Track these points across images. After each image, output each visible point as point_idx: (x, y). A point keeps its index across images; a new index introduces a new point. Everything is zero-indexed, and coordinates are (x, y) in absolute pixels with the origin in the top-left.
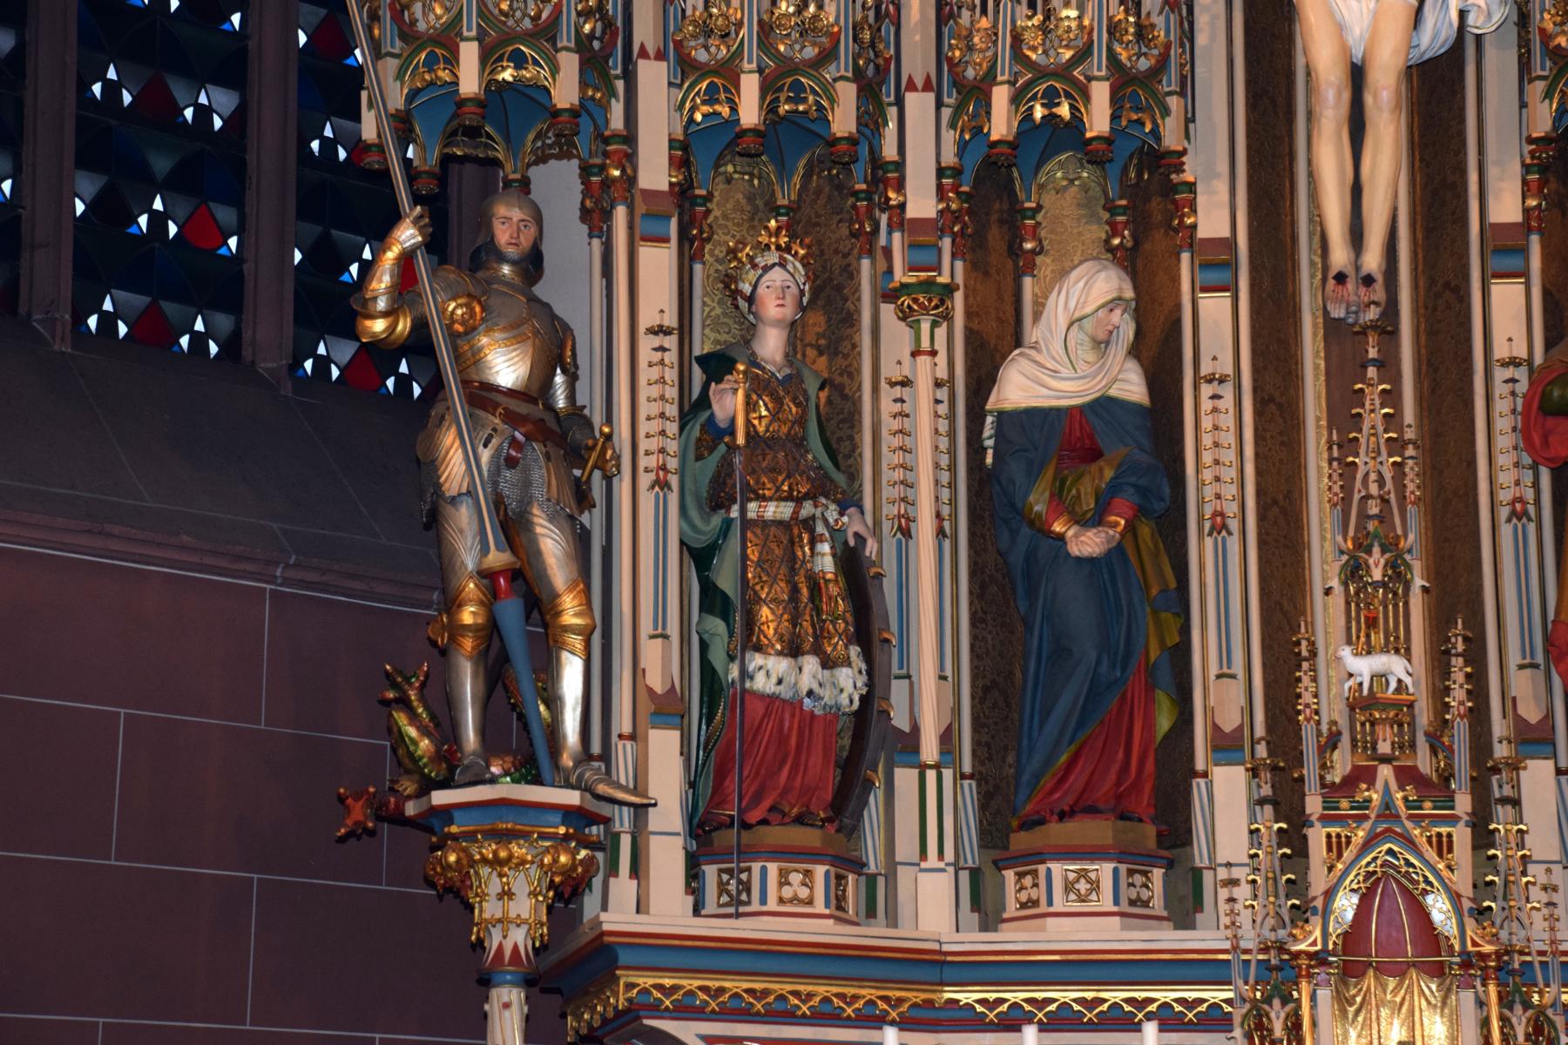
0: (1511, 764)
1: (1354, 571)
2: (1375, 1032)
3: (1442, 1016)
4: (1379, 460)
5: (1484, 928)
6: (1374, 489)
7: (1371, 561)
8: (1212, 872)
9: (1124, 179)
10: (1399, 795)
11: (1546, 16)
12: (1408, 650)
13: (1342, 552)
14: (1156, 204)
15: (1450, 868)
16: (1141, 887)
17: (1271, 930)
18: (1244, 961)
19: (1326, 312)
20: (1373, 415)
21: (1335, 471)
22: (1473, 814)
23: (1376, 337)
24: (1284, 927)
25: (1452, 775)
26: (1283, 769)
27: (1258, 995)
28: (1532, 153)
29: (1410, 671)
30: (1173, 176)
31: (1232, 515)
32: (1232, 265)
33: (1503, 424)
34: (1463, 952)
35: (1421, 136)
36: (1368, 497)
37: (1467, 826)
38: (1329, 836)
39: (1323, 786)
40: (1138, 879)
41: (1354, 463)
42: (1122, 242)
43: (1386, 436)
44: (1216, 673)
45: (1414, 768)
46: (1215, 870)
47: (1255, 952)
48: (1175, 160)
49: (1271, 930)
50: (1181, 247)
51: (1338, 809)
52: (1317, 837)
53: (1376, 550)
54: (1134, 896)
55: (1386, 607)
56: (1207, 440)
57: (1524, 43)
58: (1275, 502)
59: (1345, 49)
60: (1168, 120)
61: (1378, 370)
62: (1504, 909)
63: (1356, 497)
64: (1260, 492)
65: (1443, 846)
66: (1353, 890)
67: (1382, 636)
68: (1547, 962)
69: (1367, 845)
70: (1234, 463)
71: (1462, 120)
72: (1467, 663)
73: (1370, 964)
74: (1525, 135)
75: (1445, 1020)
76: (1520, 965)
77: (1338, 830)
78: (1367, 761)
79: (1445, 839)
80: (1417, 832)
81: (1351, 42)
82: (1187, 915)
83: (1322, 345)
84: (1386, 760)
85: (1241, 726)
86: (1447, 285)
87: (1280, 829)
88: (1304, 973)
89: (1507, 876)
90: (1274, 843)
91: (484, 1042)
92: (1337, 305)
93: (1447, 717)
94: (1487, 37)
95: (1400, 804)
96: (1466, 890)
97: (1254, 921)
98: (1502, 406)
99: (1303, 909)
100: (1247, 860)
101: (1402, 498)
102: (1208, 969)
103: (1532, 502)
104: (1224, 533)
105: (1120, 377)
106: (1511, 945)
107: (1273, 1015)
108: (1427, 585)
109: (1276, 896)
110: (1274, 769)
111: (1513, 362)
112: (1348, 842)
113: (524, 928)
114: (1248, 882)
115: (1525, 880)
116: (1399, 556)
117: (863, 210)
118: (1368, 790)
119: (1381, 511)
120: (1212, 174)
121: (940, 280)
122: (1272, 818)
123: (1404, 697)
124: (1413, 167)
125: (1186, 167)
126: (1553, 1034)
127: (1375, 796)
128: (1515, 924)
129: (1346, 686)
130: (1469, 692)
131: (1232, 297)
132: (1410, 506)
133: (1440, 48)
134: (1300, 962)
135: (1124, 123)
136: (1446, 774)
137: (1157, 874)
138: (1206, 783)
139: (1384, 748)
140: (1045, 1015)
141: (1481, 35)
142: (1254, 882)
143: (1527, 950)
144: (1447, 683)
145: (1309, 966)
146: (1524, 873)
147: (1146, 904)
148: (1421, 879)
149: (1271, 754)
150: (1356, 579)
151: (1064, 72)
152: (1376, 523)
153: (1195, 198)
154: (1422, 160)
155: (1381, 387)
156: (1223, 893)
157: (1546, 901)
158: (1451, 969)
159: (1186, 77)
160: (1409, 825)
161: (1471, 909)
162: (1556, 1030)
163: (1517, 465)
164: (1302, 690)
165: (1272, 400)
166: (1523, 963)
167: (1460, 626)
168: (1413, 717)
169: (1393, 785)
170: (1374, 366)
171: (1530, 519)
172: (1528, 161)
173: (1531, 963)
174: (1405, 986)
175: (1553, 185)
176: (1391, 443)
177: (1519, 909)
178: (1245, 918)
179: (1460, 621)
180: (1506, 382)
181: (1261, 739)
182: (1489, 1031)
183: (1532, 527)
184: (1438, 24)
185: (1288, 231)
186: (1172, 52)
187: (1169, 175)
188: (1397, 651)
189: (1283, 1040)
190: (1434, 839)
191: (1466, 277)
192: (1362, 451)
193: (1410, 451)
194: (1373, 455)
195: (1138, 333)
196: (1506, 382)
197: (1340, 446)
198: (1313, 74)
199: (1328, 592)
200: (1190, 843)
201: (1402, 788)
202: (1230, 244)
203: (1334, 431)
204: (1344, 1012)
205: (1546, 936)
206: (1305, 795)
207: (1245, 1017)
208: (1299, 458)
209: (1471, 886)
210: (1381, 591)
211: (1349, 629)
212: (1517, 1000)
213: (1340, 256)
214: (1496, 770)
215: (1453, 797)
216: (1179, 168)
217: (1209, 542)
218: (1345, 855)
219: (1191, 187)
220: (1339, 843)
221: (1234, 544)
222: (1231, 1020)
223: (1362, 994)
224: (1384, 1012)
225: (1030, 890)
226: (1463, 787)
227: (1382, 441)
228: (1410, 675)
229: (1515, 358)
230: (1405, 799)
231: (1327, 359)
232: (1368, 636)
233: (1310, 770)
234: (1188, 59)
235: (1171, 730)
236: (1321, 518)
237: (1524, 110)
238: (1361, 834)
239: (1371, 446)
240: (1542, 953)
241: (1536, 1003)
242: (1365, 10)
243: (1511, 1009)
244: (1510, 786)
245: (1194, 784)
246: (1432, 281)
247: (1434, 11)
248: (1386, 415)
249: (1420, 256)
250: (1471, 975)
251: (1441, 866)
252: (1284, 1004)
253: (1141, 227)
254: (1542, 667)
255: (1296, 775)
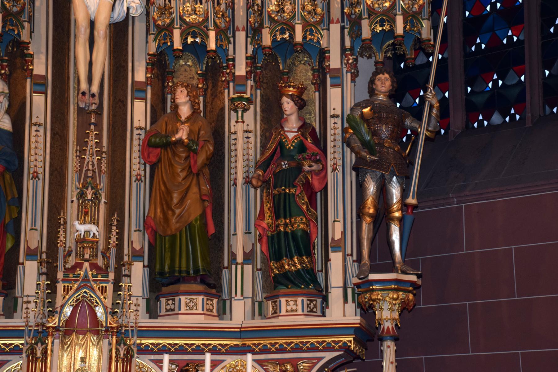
0: (129, 263)
1: (81, 195)
2: (73, 354)
3: (97, 348)
4: (93, 157)
5: (114, 319)
6: (90, 167)
7: (88, 192)
8: (22, 298)
9: (7, 50)
10: (90, 273)
11: (155, 14)
12: (98, 223)
13: (78, 188)
14: (18, 60)
15: (105, 298)
16: (210, 305)
17: (40, 319)
18: (29, 330)
19: (78, 105)
20: (92, 142)
21: (77, 160)
22: (115, 280)
23: (94, 115)
24: (46, 318)
25: (109, 266)
26: (51, 263)
27: (33, 342)
28: (149, 59)
29: (98, 230)
30: (25, 51)
31: (40, 173)
32: (45, 85)
33: (136, 149)
34: (106, 327)
35: (113, 48)
36: (88, 170)
37: (112, 284)
38: (64, 286)
39: (65, 269)
40: (209, 302)
41: (84, 158)
42: (5, 72)
43: (96, 149)
44: (30, 228)
45: (97, 264)
46: (23, 298)
47: (34, 326)
48: (26, 45)
49: (40, 319)
50: (27, 76)
51: (69, 277)
52: (60, 287)
53: (90, 188)
54: (208, 308)
55: (91, 208)
56: (33, 146)
57: (148, 21)
58: (56, 170)
59: (88, 15)
60: (23, 30)
61: (95, 126)
62: (121, 312)
63: (84, 170)
64: (51, 166)
65: (103, 290)
66: (71, 305)
67: (89, 218)
68: (133, 330)
69: (78, 290)
70: (42, 155)
71: (127, 45)
72: (117, 229)
73: (74, 331)
74: (147, 52)
75: (98, 349)
76: (125, 331)
77: (68, 284)
78: (80, 261)
79: (104, 288)
80: (95, 285)
81: (90, 12)
82: (11, 314)
83: (76, 117)
84: (87, 260)
85: (38, 247)
86: (120, 100)
87: (47, 284)
88: (50, 334)
89: (123, 301)
90: (45, 289)
91: (397, 358)
92: (82, 103)
93: (109, 247)
94: (136, 17)
95: (90, 276)
96: (109, 305)
97: (35, 316)
98: (135, 143)
99: (53, 311)
100: (35, 295)
101: (100, 171)
102: (16, 333)
103: (143, 176)
104: (37, 179)
105: (2, 120)
106: (122, 324)
107: (37, 349)
108: (106, 201)
109: (44, 307)
110: (48, 262)
111: (140, 128)
112: (71, 289)
113: (389, 321)
114: (34, 302)
115: (129, 302)
116: (98, 191)
117: (316, 76)
118: (80, 271)
119: (92, 175)
120: (40, 52)
121: (246, 96)
122: (45, 280)
123: (95, 239)
124: (110, 58)
125: (30, 48)
126: (132, 354)
127: (82, 273)
128: (124, 317)
129: (76, 235)
130: (117, 238)
131: (45, 96)
132: (102, 174)
133: (120, 19)
134: (49, 330)
135: (7, 29)
136: (107, 266)
137: (215, 301)
138: (23, 267)
139: (87, 256)
140: (208, 349)
141: (134, 17)
142: (36, 302)
143: (127, 326)
144: (110, 235)
145: (52, 332)
146: (129, 300)
147: (211, 311)
148: (95, 302)
149: (47, 257)
150: (82, 198)
151: (198, 25)
152: (90, 179)
153: (33, 60)
154: (113, 57)
155: (95, 133)
156: (25, 306)
157: (135, 309)
158: (102, 332)
159: (31, 16)
160: (92, 283)
161: (110, 312)
162: (133, 352)
163: (139, 163)
164: (60, 235)
165: (57, 133)
166: (125, 330)
167: (116, 216)
168: (98, 246)
169: (89, 269)
170: (93, 125)
171: (142, 181)
172: (148, 61)
173: (128, 330)
174: (85, 338)
175: (156, 70)
176: (97, 152)
177: (126, 312)
178: (32, 315)
179: (116, 214)
180: (137, 135)
181: (44, 252)
182: (112, 353)
183: (142, 184)
184: (120, 11)
185: (66, 75)
186: (26, 7)
187: (23, 51)
188: (94, 223)
189: (40, 357)
190: (101, 288)
191: (126, 98)
192: (87, 154)
193: (104, 155)
194: (91, 156)
195: (9, 106)
196: (137, 135)
197: (80, 152)
198: (77, 22)
199: (72, 202)
200: (15, 288)
201: (91, 270)
202: (45, 77)
203: (78, 146)
204: (63, 347)
205: (134, 321)
206: (57, 272)
207: (27, 350)
208: (66, 155)
209: (111, 304)
210: (90, 202)
211: (78, 215)
212: (122, 342)
213: (84, 86)
214: (124, 265)
215: (108, 274)
216: (28, 49)
217: (31, 182)
218: (70, 293)
219: (32, 56)
220: (68, 289)
221: (40, 183)
222: (22, 351)
223: (70, 341)
224: (77, 347)
225: (171, 305)
226: (112, 271)
227: (94, 151)
228: (98, 232)
229: (141, 127)
230: (92, 274)
231: (78, 121)
232: (85, 218)
233: (60, 263)
234: (32, 10)
235: (12, 248)
236: (72, 176)
237: (147, 44)
238: (76, 286)
239: (91, 152)
240: (132, 327)
241: (128, 343)
242: (95, 2)
243: (120, 346)
244: (128, 270)
245: (18, 267)
246: (115, 98)
247: (119, 6)
248: (96, 142)
249: (111, 89)
250: (108, 334)
251: (102, 297)
252: (42, 345)
253: (13, 67)
254: (142, 231)
255: (55, 265)
